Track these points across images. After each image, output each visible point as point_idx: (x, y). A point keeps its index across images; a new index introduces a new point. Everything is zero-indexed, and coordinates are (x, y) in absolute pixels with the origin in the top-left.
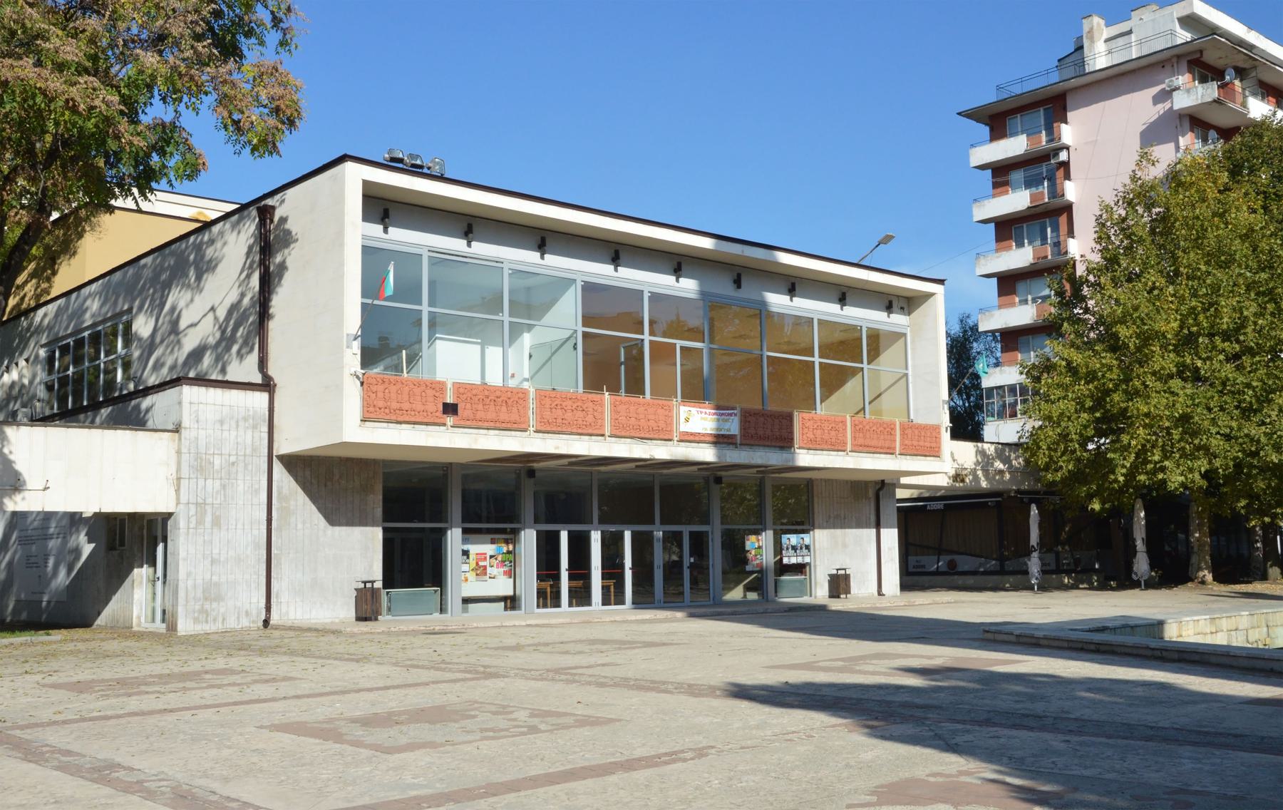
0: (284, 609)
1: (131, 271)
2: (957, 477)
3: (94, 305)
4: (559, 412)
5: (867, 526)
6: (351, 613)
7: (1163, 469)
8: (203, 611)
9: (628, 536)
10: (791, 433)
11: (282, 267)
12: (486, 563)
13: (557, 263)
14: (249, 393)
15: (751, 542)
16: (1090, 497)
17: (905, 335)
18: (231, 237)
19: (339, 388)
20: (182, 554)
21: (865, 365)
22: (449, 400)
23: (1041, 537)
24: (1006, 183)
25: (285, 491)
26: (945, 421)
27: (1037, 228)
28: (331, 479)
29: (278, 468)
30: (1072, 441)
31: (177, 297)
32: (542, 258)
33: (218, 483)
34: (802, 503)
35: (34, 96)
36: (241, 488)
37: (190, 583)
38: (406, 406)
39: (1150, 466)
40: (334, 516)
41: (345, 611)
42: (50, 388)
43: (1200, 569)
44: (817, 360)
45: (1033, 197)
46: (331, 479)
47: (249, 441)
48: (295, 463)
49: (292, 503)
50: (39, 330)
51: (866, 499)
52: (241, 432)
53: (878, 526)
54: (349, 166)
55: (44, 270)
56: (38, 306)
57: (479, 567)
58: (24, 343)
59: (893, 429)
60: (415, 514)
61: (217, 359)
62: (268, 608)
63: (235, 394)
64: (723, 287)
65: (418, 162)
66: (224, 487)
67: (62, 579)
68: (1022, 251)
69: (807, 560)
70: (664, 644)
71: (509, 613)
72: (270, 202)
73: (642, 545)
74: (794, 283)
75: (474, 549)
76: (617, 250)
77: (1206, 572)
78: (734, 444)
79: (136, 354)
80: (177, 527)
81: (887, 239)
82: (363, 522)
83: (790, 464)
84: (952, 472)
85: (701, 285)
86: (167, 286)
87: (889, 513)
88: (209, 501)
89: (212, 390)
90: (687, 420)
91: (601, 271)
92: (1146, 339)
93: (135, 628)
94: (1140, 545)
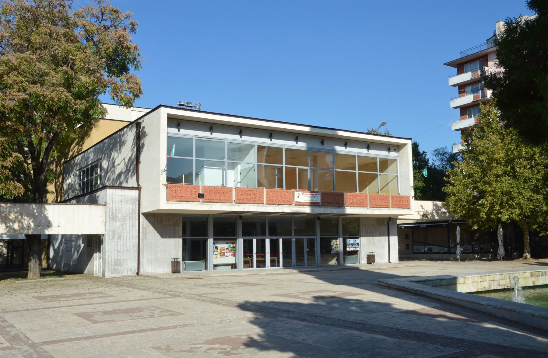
0: (145, 268)
1: (102, 144)
2: (424, 215)
3: (92, 156)
4: (245, 196)
5: (384, 235)
6: (170, 270)
7: (501, 213)
8: (114, 269)
9: (281, 241)
10: (343, 201)
11: (143, 145)
12: (225, 251)
13: (247, 139)
14: (131, 191)
15: (334, 242)
16: (474, 224)
17: (396, 160)
18: (129, 133)
19: (158, 189)
20: (107, 249)
21: (378, 173)
22: (201, 192)
23: (461, 238)
24: (464, 92)
25: (145, 226)
26: (412, 193)
27: (477, 110)
28: (162, 222)
29: (142, 217)
30: (463, 201)
31: (114, 154)
32: (241, 137)
33: (120, 223)
34: (355, 227)
35: (40, 97)
36: (128, 225)
37: (110, 259)
38: (184, 195)
39: (496, 212)
40: (164, 234)
41: (168, 269)
42: (80, 185)
43: (525, 253)
44: (357, 171)
45: (474, 97)
46: (162, 222)
47: (131, 208)
48: (148, 216)
49: (148, 230)
50: (76, 165)
51: (384, 226)
52: (128, 205)
53: (389, 235)
54: (162, 109)
55: (80, 142)
56: (79, 155)
57: (220, 253)
58: (73, 168)
59: (388, 198)
60: (196, 234)
61: (125, 177)
62: (139, 268)
63: (126, 191)
64: (317, 145)
65: (191, 105)
66: (122, 225)
67: (76, 256)
68: (471, 119)
69: (358, 249)
70: (259, 285)
71: (234, 270)
72: (140, 121)
73: (287, 244)
74: (346, 142)
75: (220, 246)
76: (271, 133)
77: (527, 254)
78: (319, 206)
79: (103, 174)
80: (105, 238)
81: (384, 124)
82: (174, 237)
83: (343, 213)
84: (422, 213)
85: (307, 144)
86: (111, 150)
87: (394, 229)
88: (117, 230)
89: (117, 190)
90: (298, 197)
91: (265, 141)
92: (492, 160)
93: (95, 275)
94: (500, 243)
